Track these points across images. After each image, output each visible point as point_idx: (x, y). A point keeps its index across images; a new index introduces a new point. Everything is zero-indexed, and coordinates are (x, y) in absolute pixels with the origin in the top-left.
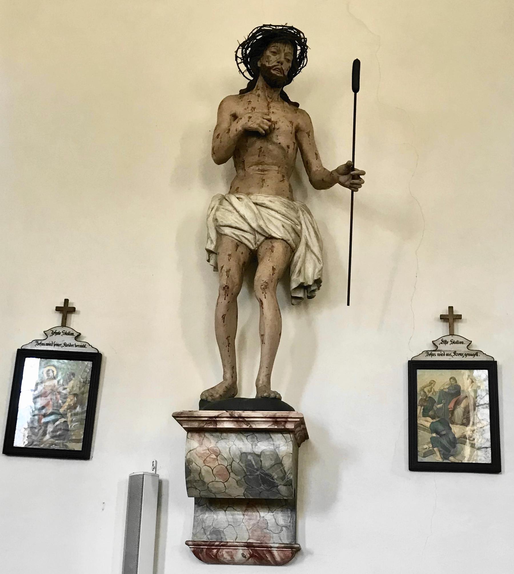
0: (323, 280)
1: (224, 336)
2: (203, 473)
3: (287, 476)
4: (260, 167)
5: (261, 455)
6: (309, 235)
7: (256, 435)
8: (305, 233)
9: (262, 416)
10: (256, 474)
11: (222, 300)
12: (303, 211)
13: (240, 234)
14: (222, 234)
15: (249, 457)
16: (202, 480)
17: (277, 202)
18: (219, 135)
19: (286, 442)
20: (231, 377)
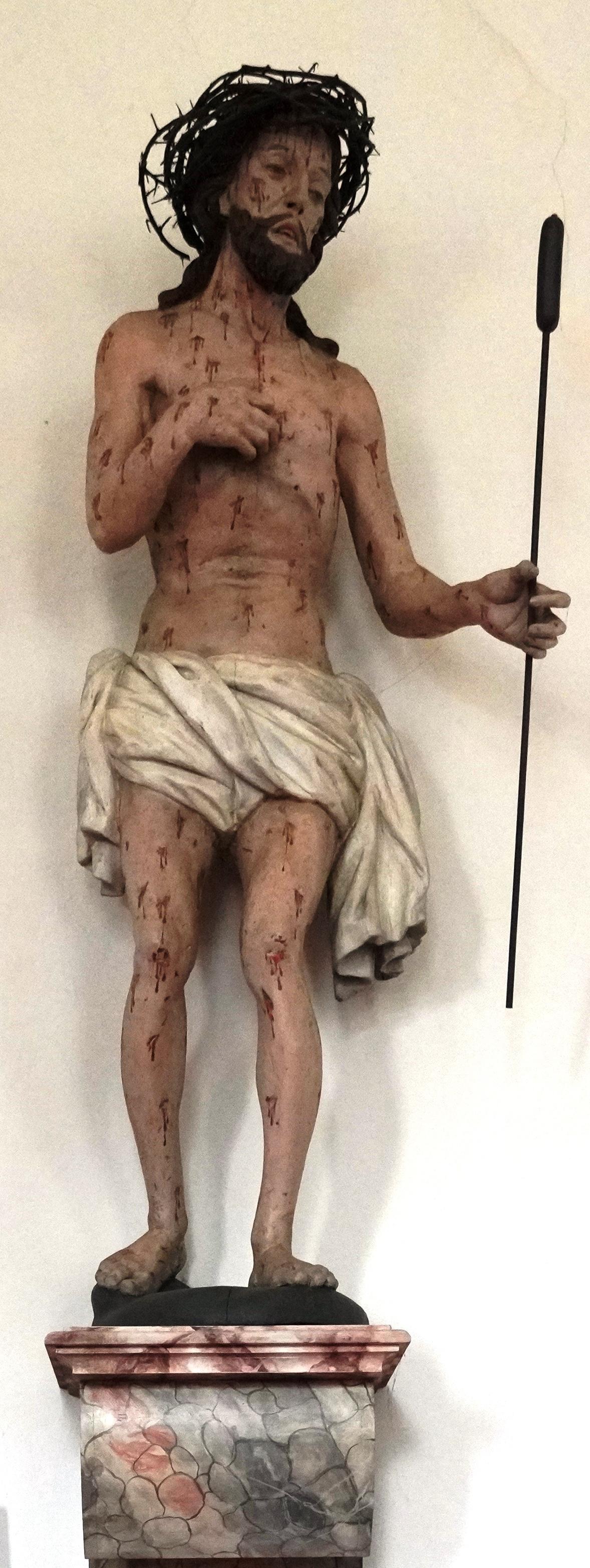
0: (429, 927)
1: (151, 1098)
2: (133, 1497)
3: (361, 1499)
4: (235, 563)
5: (288, 1446)
6: (388, 787)
7: (271, 1390)
8: (374, 779)
9: (296, 1341)
10: (276, 1496)
11: (146, 990)
12: (363, 708)
13: (192, 784)
14: (132, 783)
15: (258, 1452)
16: (128, 1516)
17: (295, 683)
18: (108, 453)
19: (358, 1409)
20: (173, 1217)
